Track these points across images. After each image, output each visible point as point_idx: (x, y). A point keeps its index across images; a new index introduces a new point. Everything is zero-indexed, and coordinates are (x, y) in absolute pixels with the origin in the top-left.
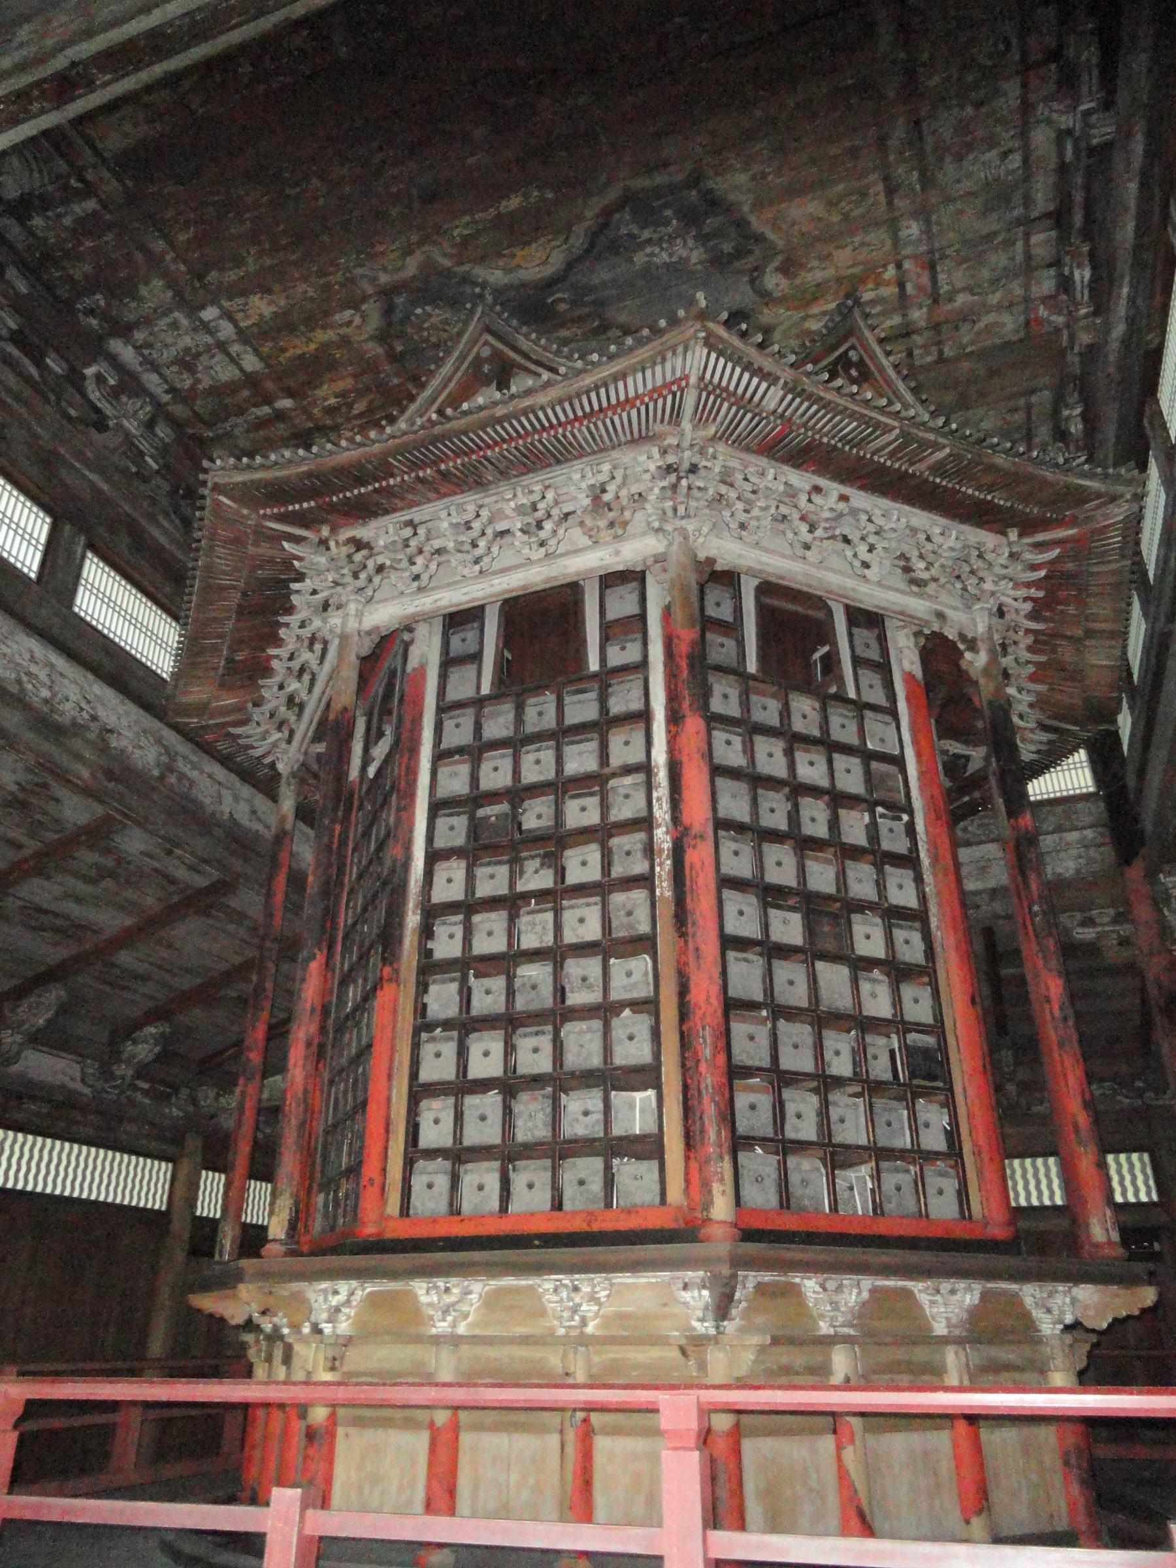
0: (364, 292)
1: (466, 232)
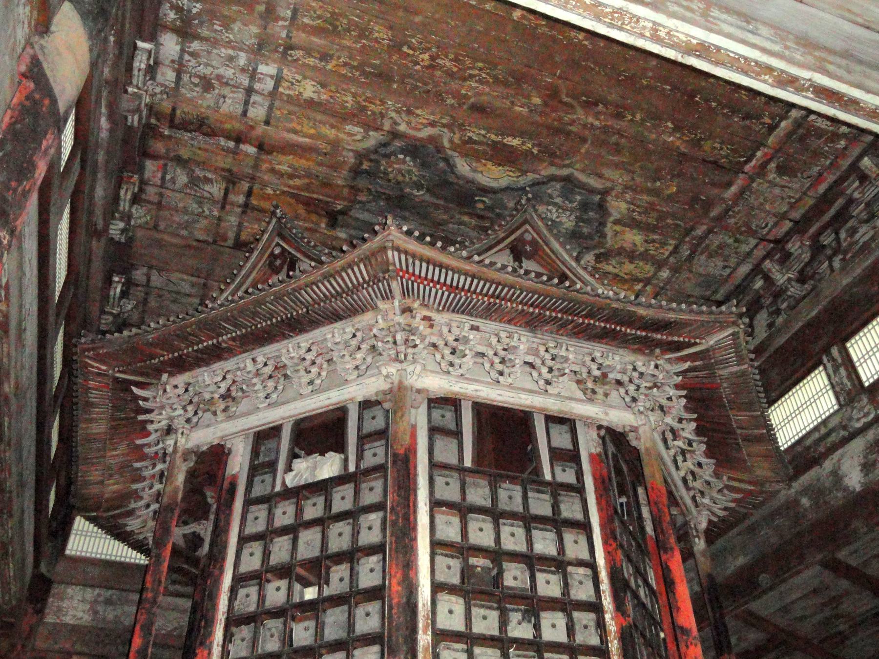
0: (382, 124)
1: (474, 138)
